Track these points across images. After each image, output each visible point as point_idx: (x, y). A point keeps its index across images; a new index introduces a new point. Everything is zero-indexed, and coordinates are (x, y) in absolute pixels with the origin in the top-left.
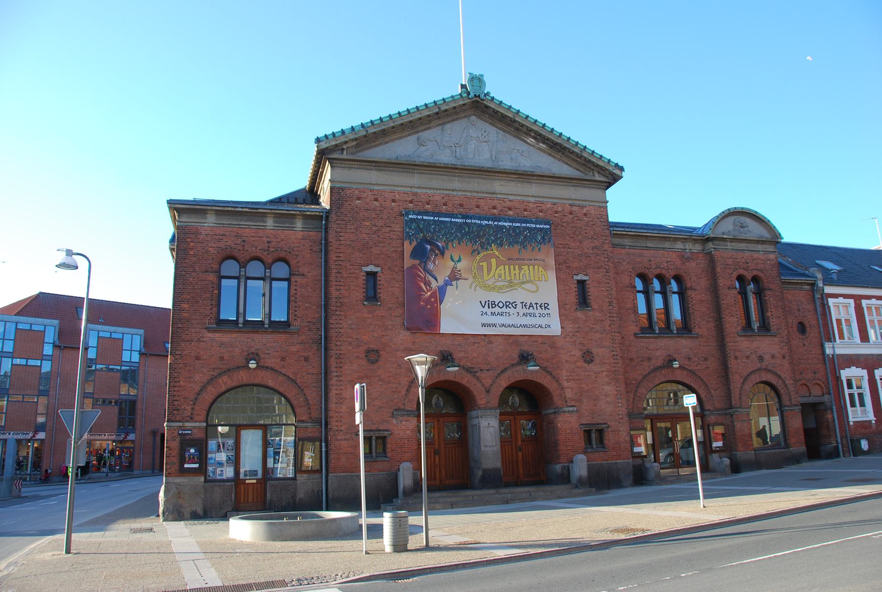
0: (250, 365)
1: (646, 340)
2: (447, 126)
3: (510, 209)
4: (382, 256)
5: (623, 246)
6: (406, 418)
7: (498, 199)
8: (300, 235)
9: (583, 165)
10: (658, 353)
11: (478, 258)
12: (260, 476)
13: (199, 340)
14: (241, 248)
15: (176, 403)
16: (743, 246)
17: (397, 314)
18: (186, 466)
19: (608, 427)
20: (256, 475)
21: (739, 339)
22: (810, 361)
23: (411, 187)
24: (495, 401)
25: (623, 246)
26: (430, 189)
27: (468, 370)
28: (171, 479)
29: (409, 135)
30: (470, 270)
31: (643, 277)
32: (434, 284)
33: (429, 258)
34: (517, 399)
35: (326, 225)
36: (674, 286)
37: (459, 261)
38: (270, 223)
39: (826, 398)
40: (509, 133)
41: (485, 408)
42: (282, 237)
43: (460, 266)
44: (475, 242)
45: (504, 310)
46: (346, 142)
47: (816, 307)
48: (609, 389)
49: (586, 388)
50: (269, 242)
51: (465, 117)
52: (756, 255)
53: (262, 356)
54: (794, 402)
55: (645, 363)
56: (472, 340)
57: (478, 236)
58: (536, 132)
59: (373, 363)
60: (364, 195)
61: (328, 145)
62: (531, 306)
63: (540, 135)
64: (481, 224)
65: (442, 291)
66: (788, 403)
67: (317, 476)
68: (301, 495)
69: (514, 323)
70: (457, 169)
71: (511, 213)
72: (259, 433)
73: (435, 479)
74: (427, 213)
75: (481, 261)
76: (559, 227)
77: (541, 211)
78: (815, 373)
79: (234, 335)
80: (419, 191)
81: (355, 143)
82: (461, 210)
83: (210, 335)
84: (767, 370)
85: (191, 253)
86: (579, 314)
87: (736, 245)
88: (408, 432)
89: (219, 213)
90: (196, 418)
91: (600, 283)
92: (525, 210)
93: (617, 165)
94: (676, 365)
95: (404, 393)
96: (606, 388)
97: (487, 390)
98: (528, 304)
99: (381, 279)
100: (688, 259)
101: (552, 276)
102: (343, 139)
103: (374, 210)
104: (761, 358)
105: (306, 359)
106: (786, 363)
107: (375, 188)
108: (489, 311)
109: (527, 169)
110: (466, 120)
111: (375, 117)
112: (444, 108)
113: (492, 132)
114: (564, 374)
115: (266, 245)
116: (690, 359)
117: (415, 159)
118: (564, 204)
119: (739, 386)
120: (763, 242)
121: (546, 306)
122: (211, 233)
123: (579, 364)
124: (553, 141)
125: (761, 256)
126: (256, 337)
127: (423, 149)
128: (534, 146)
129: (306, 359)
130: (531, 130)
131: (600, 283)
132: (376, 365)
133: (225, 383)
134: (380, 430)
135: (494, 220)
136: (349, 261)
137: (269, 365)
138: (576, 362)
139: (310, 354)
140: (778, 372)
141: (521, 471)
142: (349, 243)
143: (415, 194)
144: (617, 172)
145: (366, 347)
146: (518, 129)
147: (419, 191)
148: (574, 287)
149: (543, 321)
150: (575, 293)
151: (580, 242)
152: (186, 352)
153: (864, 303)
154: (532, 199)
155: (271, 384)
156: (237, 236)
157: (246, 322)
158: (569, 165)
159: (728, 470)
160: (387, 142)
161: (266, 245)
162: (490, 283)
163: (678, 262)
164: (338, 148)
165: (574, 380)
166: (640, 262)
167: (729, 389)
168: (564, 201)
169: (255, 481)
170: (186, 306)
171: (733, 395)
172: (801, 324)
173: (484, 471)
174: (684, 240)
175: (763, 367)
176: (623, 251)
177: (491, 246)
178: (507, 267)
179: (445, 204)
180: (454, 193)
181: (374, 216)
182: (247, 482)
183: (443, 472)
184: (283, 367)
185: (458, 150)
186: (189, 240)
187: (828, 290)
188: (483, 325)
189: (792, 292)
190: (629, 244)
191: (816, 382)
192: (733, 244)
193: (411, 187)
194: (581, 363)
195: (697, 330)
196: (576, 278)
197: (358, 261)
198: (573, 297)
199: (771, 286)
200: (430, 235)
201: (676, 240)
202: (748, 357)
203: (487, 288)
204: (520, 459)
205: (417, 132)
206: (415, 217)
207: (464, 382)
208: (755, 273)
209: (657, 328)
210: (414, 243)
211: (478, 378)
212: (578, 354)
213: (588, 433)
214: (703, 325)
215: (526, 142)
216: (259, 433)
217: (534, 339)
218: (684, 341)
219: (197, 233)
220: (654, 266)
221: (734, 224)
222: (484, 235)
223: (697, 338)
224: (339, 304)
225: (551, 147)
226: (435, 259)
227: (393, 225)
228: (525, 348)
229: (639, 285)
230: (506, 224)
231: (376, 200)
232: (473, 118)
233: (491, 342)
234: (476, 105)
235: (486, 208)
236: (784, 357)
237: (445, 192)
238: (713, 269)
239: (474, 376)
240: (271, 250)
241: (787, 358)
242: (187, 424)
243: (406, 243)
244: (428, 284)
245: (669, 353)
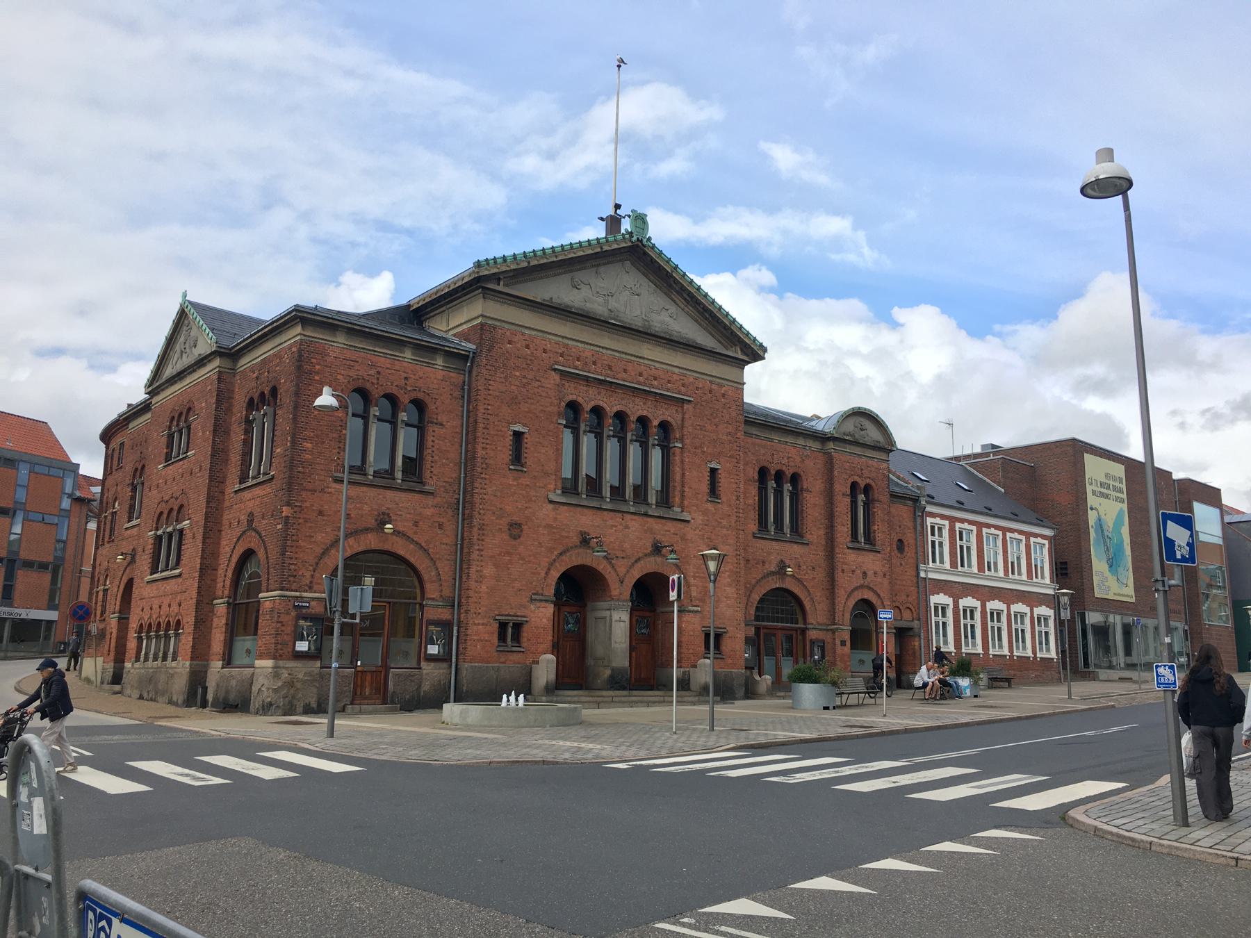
2: (602, 269)
3: (655, 379)
13: (322, 491)
16: (857, 450)
35: (471, 367)
39: (915, 624)
42: (421, 374)
50: (406, 378)
60: (515, 339)
67: (445, 665)
68: (426, 687)
71: (656, 383)
77: (683, 385)
86: (709, 506)
90: (315, 587)
93: (761, 345)
95: (543, 575)
99: (529, 441)
104: (865, 573)
105: (441, 526)
106: (886, 582)
112: (606, 248)
133: (351, 547)
143: (566, 346)
144: (761, 353)
146: (670, 286)
152: (307, 504)
153: (985, 530)
161: (403, 382)
167: (833, 604)
170: (309, 445)
172: (900, 541)
184: (415, 533)
187: (929, 509)
199: (881, 498)
202: (853, 571)
205: (572, 271)
207: (600, 568)
208: (868, 481)
213: (503, 626)
231: (527, 347)
232: (628, 264)
238: (831, 471)
242: (305, 594)
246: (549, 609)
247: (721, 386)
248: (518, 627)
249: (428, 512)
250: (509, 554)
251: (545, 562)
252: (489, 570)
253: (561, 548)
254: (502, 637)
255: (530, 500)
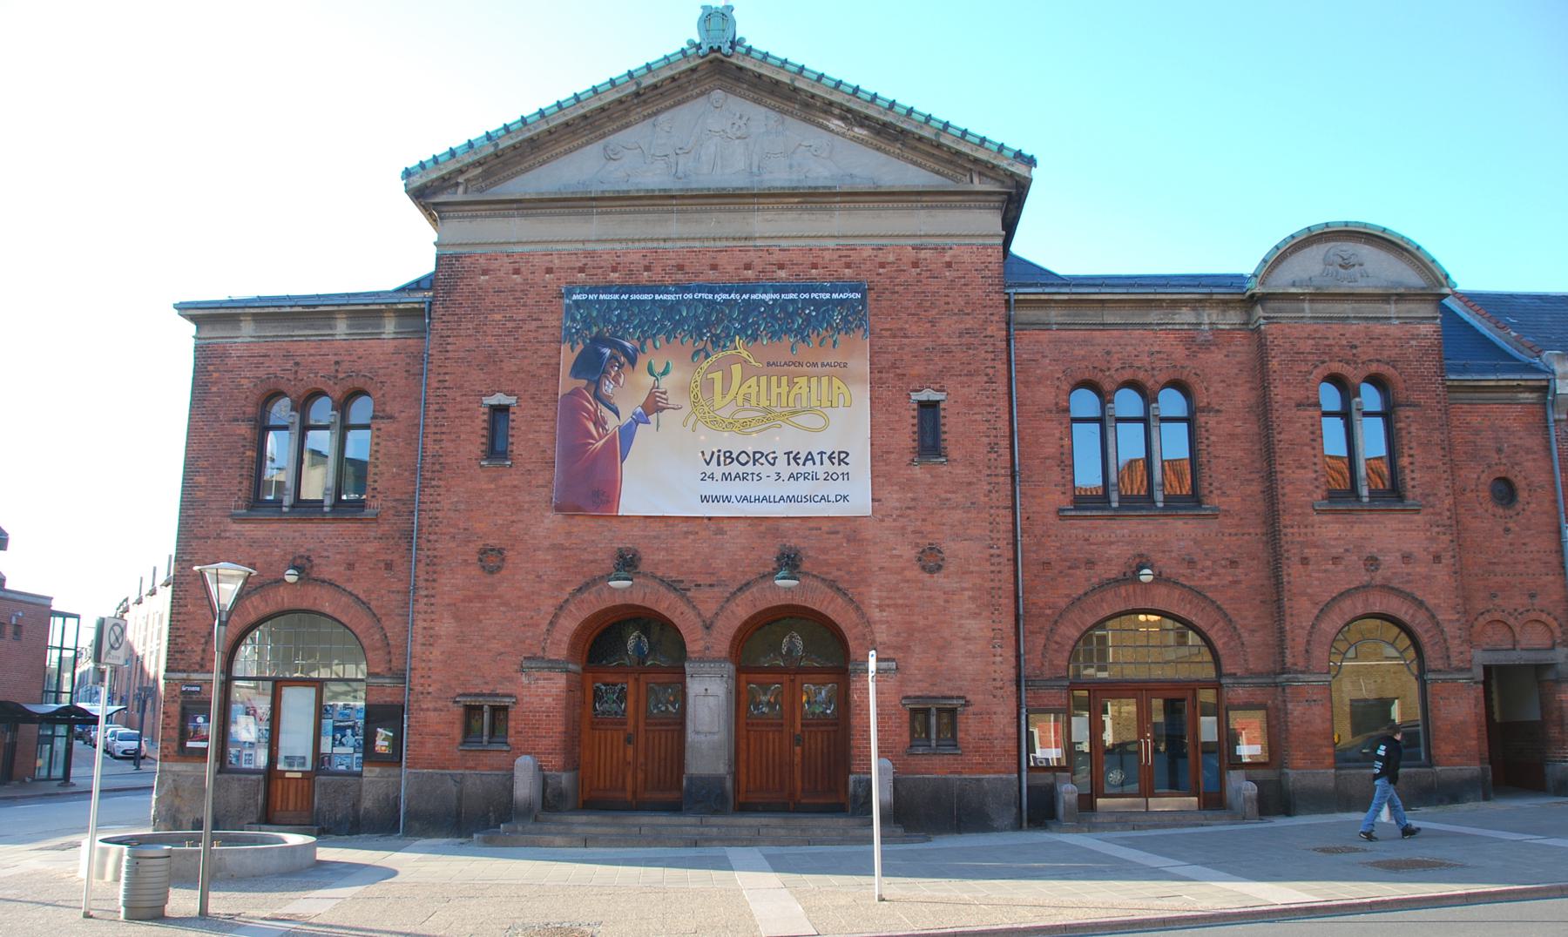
0: (287, 578)
1: (1085, 523)
2: (662, 118)
3: (781, 267)
4: (521, 375)
5: (1045, 326)
6: (546, 673)
7: (757, 249)
8: (389, 347)
9: (951, 162)
10: (1112, 551)
11: (705, 365)
12: (309, 767)
13: (219, 537)
14: (291, 377)
15: (179, 640)
17: (541, 482)
18: (189, 744)
19: (967, 704)
20: (304, 764)
21: (1317, 518)
22: (1521, 568)
23: (583, 242)
24: (722, 646)
25: (1045, 326)
26: (620, 241)
27: (672, 585)
28: (167, 765)
29: (588, 143)
30: (685, 389)
31: (1336, 380)
32: (613, 423)
33: (606, 373)
34: (799, 643)
36: (1370, 398)
37: (665, 373)
38: (341, 328)
40: (791, 114)
41: (701, 660)
42: (361, 351)
43: (665, 383)
44: (701, 335)
45: (749, 468)
46: (461, 171)
47: (1548, 441)
48: (976, 627)
49: (922, 623)
50: (337, 363)
51: (702, 94)
52: (1378, 328)
53: (316, 561)
54: (1455, 663)
55: (1078, 572)
56: (684, 527)
57: (708, 324)
58: (841, 106)
59: (492, 572)
61: (424, 180)
62: (810, 457)
63: (849, 110)
64: (714, 302)
65: (627, 434)
66: (1439, 664)
68: (367, 803)
69: (771, 495)
70: (673, 197)
71: (782, 274)
72: (310, 693)
73: (624, 789)
74: (607, 289)
75: (710, 370)
76: (887, 295)
77: (848, 266)
78: (1532, 596)
79: (275, 526)
80: (598, 247)
81: (480, 170)
82: (680, 276)
83: (236, 527)
84: (1387, 588)
85: (214, 389)
86: (917, 471)
87: (1324, 309)
88: (547, 700)
89: (258, 318)
91: (970, 405)
92: (814, 266)
93: (1019, 155)
94: (1146, 576)
95: (544, 627)
96: (972, 625)
97: (709, 627)
98: (803, 456)
99: (516, 417)
100: (1206, 346)
101: (861, 398)
102: (452, 166)
103: (513, 290)
105: (389, 566)
106: (1442, 574)
107: (518, 249)
108: (719, 471)
109: (820, 183)
110: (702, 100)
111: (512, 118)
112: (650, 81)
113: (758, 116)
114: (873, 596)
115: (333, 368)
116: (1191, 563)
117: (593, 188)
118: (902, 247)
119: (1307, 624)
120: (1401, 297)
121: (841, 458)
122: (246, 353)
123: (908, 574)
124: (877, 121)
125: (1394, 329)
126: (310, 528)
127: (612, 165)
128: (843, 135)
129: (389, 566)
130: (831, 104)
131: (970, 405)
132: (497, 576)
133: (255, 608)
134: (497, 695)
135: (741, 291)
136: (461, 387)
137: (327, 577)
138: (903, 569)
139: (395, 557)
140: (1419, 594)
141: (799, 784)
142: (462, 355)
143: (588, 254)
144: (1019, 169)
145: (480, 544)
147: (598, 247)
148: (909, 417)
149: (839, 487)
150: (910, 429)
151: (933, 323)
154: (831, 244)
155: (328, 609)
156: (287, 356)
157: (298, 502)
158: (920, 165)
159: (1252, 808)
160: (544, 162)
162: (725, 413)
163: (1180, 352)
164: (446, 182)
165: (896, 606)
166: (1084, 358)
168: (902, 242)
169: (299, 775)
171: (1289, 643)
173: (691, 779)
174: (1196, 305)
175: (1378, 580)
176: (1045, 336)
177: (733, 341)
178: (763, 379)
179: (647, 268)
180: (669, 245)
181: (511, 302)
182: (288, 775)
183: (641, 776)
184: (350, 580)
185: (682, 160)
186: (211, 368)
188: (704, 499)
189: (1483, 408)
190: (1060, 320)
191: (1533, 615)
192: (1320, 306)
193: (583, 242)
194: (915, 573)
195: (1215, 500)
196: (915, 396)
197: (478, 388)
198: (905, 437)
200: (615, 326)
201: (1175, 304)
202: (1336, 560)
203: (715, 423)
204: (797, 759)
205: (604, 136)
206: (584, 297)
207: (661, 608)
209: (1365, 492)
210: (579, 348)
211: (689, 601)
212: (909, 553)
213: (472, 711)
214: (1232, 492)
215: (826, 128)
216: (310, 693)
217: (812, 524)
218: (1179, 524)
219: (224, 355)
220: (1118, 365)
221: (1327, 263)
222: (719, 321)
223: (1216, 517)
224: (437, 467)
225: (878, 133)
226: (618, 374)
227: (544, 317)
228: (793, 542)
229: (1330, 397)
230: (767, 297)
231: (517, 272)
232: (718, 94)
233: (720, 531)
234: (718, 68)
235: (730, 268)
236: (1437, 559)
237: (650, 245)
239: (683, 596)
240: (341, 376)
241: (1447, 559)
242: (194, 676)
243: (565, 348)
244: (600, 423)
245: (1142, 549)
246: (559, 682)
247: (941, 250)
248: (499, 712)
249: (369, 548)
250: (481, 598)
251: (548, 606)
252: (446, 626)
253: (581, 580)
254: (468, 730)
255: (520, 509)
